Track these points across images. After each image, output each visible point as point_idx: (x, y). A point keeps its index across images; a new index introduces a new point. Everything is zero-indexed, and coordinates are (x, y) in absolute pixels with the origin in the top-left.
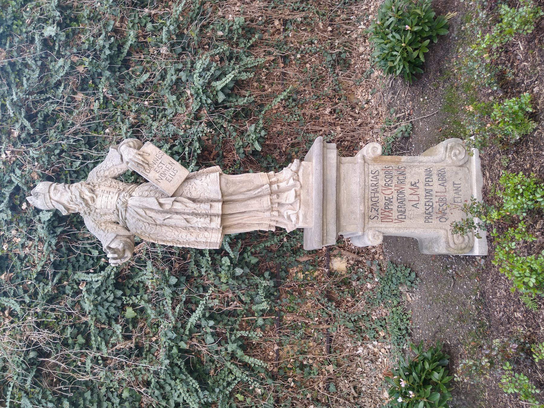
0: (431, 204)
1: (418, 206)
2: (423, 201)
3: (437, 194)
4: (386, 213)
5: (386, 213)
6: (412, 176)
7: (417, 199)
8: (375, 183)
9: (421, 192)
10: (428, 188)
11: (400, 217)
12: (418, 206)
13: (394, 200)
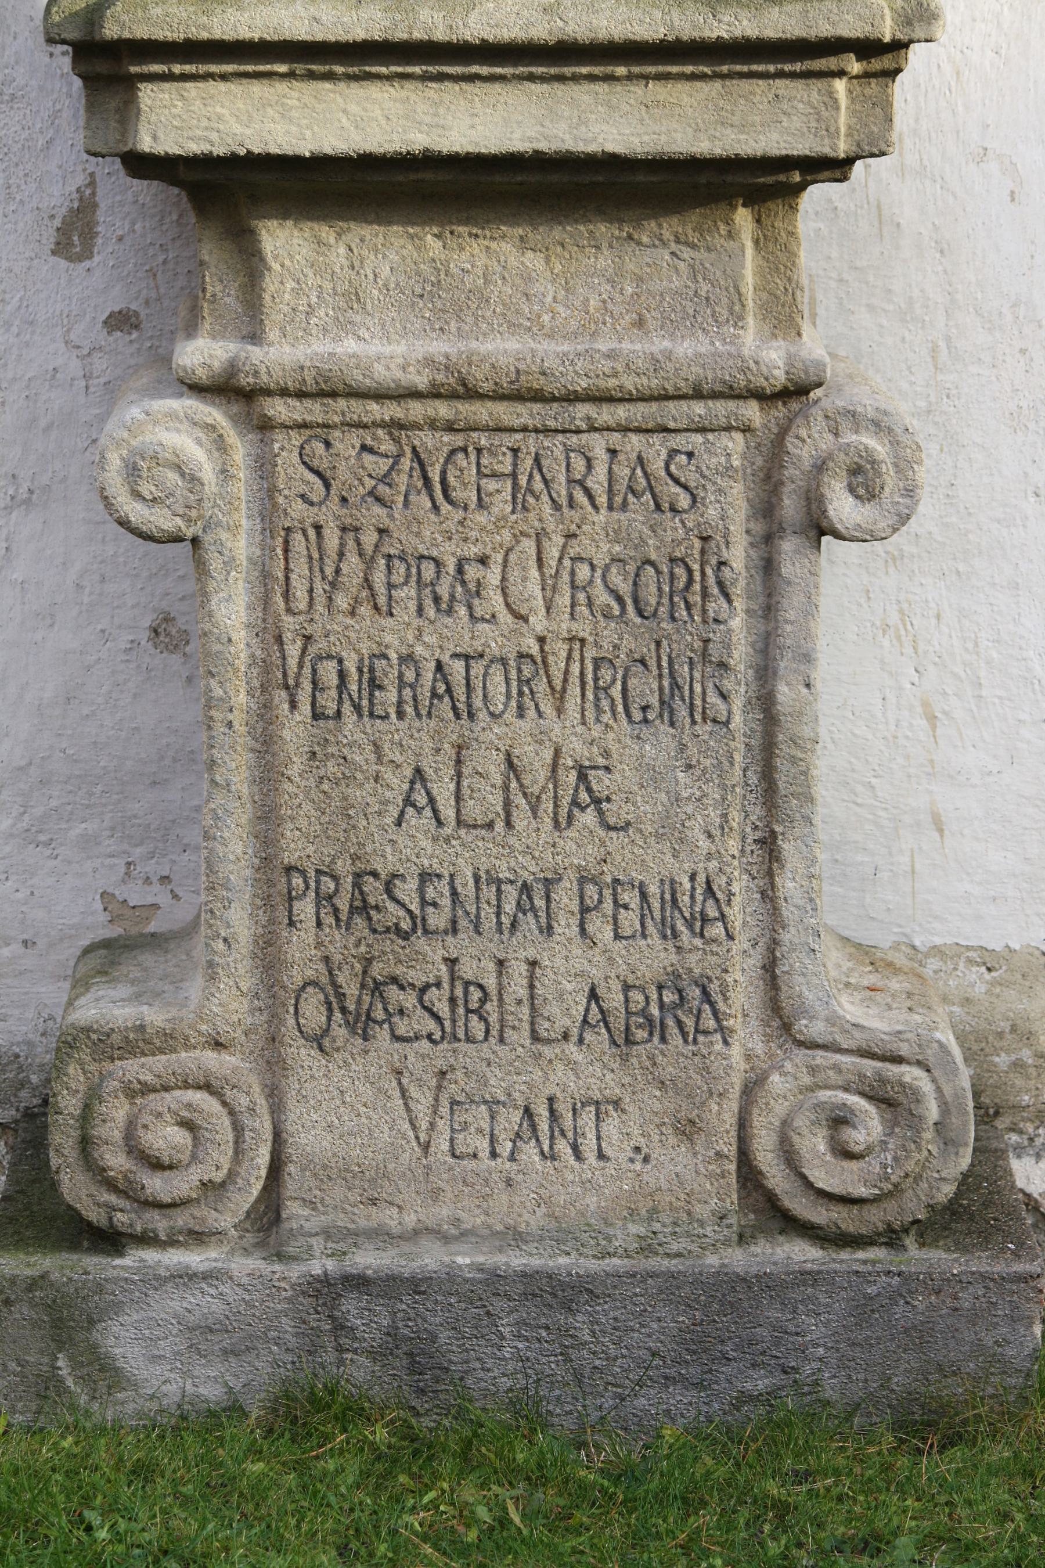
0: (437, 920)
1: (419, 822)
2: (464, 859)
3: (518, 970)
4: (352, 563)
5: (352, 563)
6: (653, 777)
7: (472, 810)
8: (598, 481)
9: (532, 846)
10: (565, 897)
11: (329, 672)
12: (419, 822)
13: (458, 631)
